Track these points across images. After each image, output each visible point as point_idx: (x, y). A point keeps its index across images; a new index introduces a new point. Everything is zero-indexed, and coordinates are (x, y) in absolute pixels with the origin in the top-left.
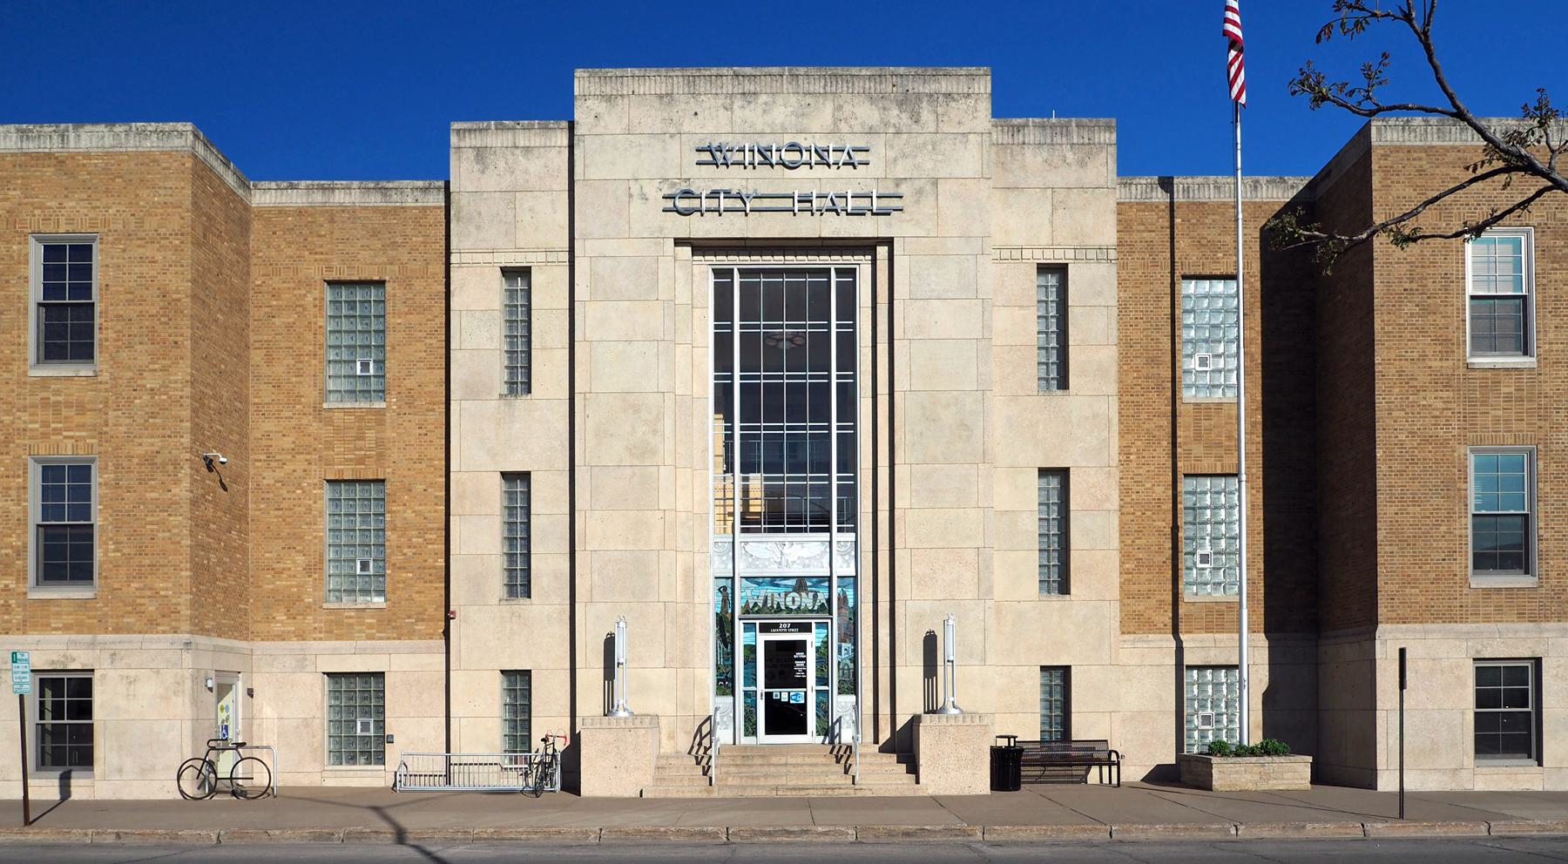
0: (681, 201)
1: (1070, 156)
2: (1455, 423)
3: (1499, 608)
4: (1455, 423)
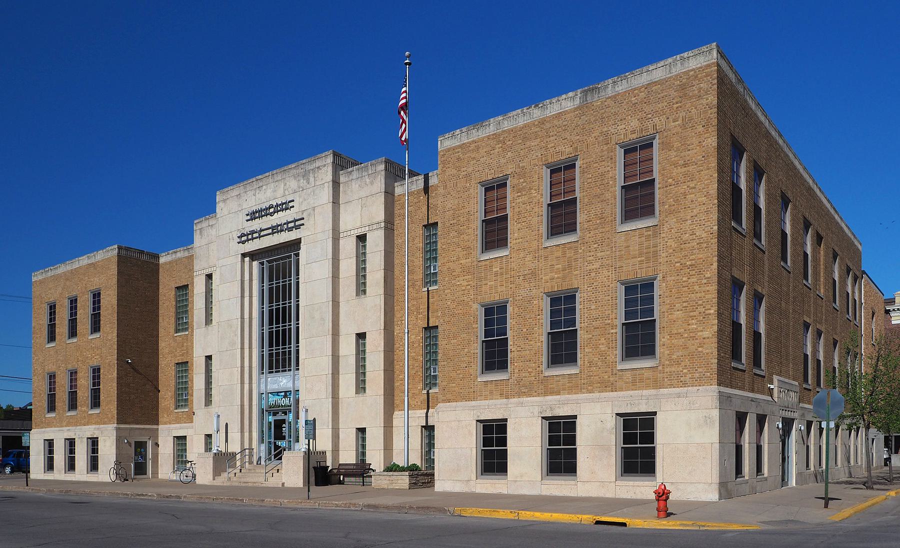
0: (245, 237)
1: (368, 180)
2: (472, 292)
3: (491, 393)
4: (472, 292)
